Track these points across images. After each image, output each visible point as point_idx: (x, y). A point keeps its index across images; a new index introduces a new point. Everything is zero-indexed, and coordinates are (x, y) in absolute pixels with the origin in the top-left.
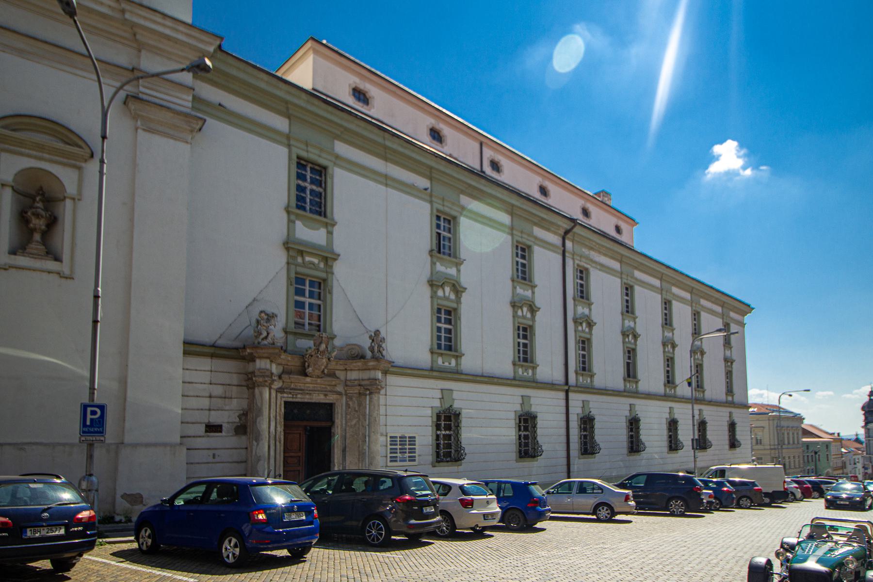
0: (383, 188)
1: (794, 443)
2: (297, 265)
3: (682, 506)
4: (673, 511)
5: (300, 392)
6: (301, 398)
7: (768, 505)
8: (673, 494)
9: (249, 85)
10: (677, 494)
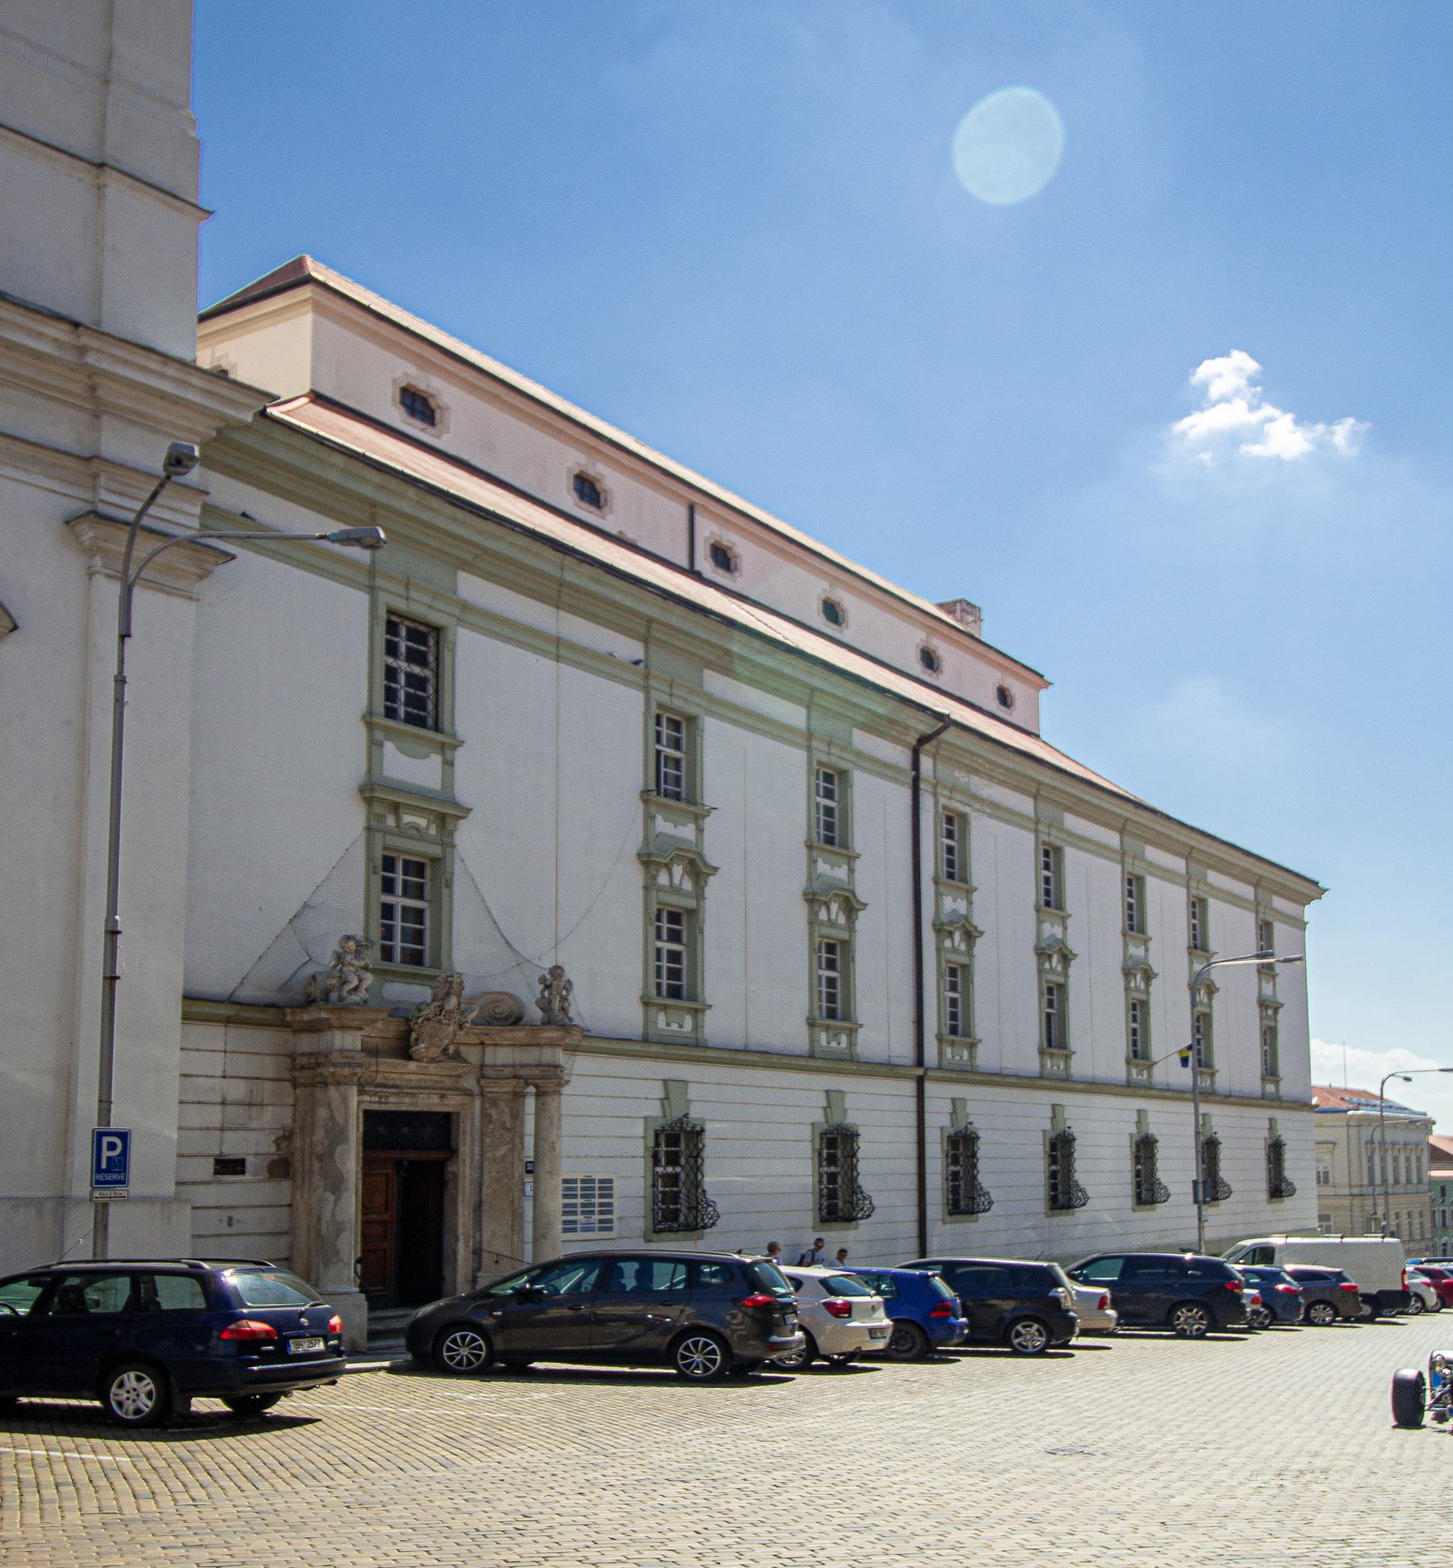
0: (550, 664)
1: (1409, 1181)
2: (387, 832)
3: (1201, 1318)
4: (1183, 1329)
5: (395, 1091)
6: (396, 1103)
7: (1369, 1320)
8: (1182, 1298)
9: (306, 476)
10: (1189, 1297)
